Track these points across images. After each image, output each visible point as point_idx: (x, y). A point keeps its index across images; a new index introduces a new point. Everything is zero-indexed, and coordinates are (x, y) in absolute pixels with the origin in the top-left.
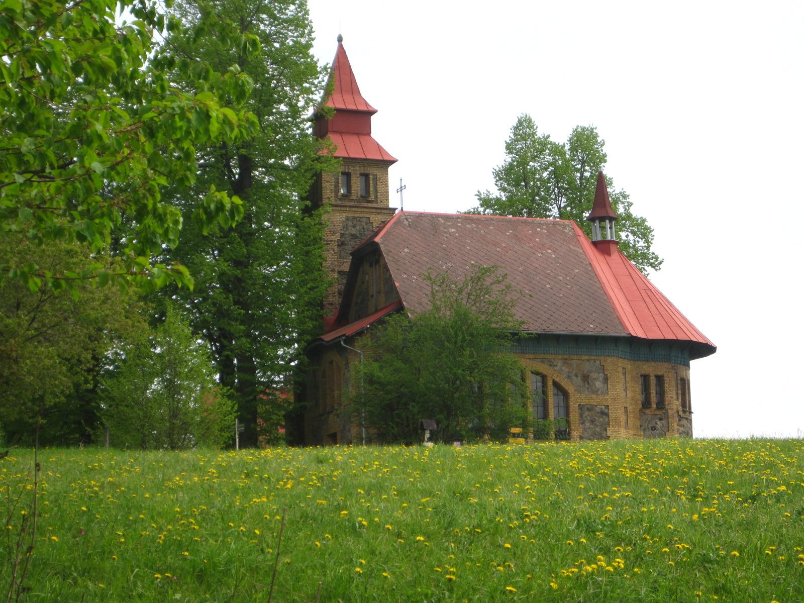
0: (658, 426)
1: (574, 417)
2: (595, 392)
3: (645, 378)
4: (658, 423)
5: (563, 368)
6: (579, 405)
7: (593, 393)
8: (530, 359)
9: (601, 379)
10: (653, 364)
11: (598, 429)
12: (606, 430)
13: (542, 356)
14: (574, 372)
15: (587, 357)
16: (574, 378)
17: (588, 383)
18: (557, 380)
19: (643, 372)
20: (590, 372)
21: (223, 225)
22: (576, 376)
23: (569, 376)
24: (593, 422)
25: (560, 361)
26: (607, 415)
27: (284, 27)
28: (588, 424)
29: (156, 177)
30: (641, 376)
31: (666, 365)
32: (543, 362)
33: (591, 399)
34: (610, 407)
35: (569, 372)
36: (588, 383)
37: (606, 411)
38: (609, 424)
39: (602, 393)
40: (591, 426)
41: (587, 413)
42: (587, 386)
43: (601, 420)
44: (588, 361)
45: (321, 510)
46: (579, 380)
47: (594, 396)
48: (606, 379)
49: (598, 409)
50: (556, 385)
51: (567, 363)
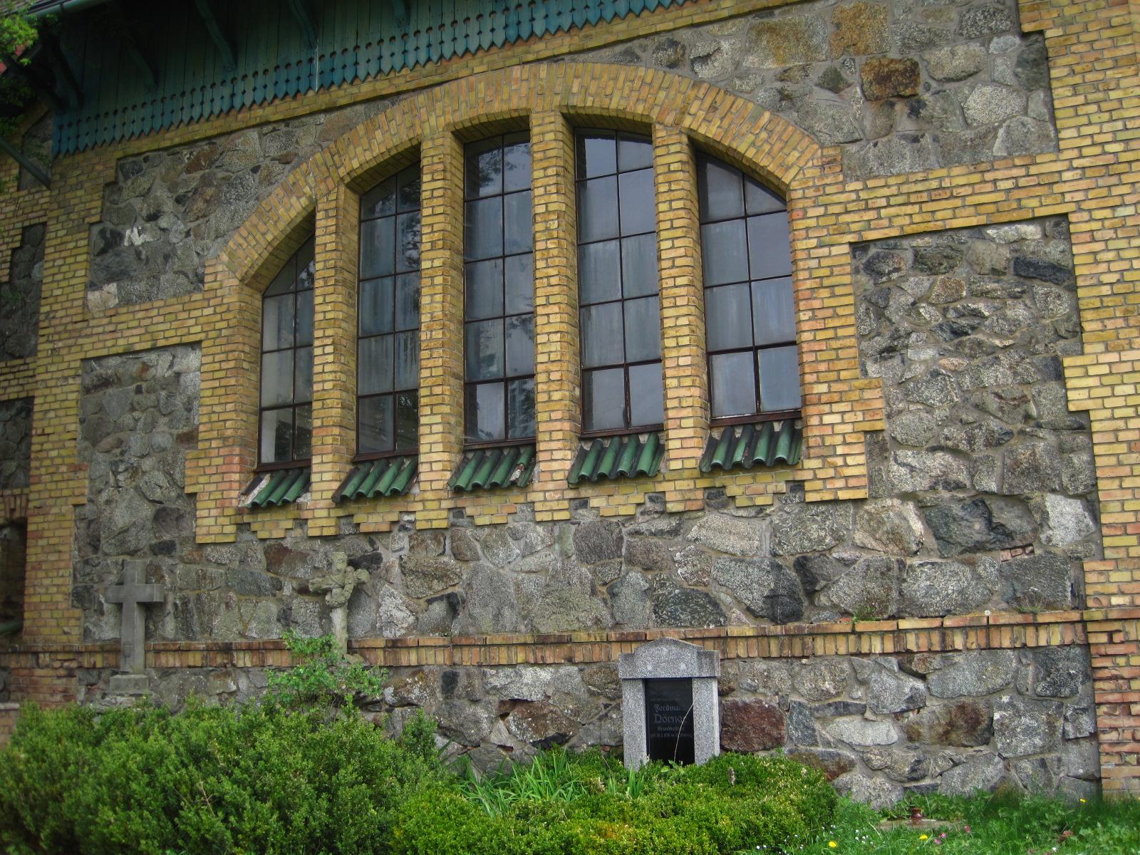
1: (825, 311)
2: (973, 149)
5: (751, 61)
6: (859, 247)
7: (948, 159)
8: (554, 59)
9: (1004, 68)
11: (997, 376)
12: (1058, 374)
13: (621, 29)
14: (819, 69)
16: (822, 97)
17: (916, 109)
18: (710, 131)
19: (535, 121)
20: (931, 44)
21: (473, 464)
22: (834, 83)
23: (784, 96)
24: (957, 333)
25: (730, 27)
26: (1062, 275)
27: (150, 680)
28: (922, 355)
32: (627, 51)
34: (1079, 224)
35: (784, 76)
36: (916, 109)
37: (1054, 251)
38: (1077, 331)
39: (1016, 147)
40: (950, 362)
41: (916, 284)
42: (907, 125)
43: (1019, 311)
47: (959, 176)
48: (1036, 65)
49: (993, 249)
51: (771, 30)
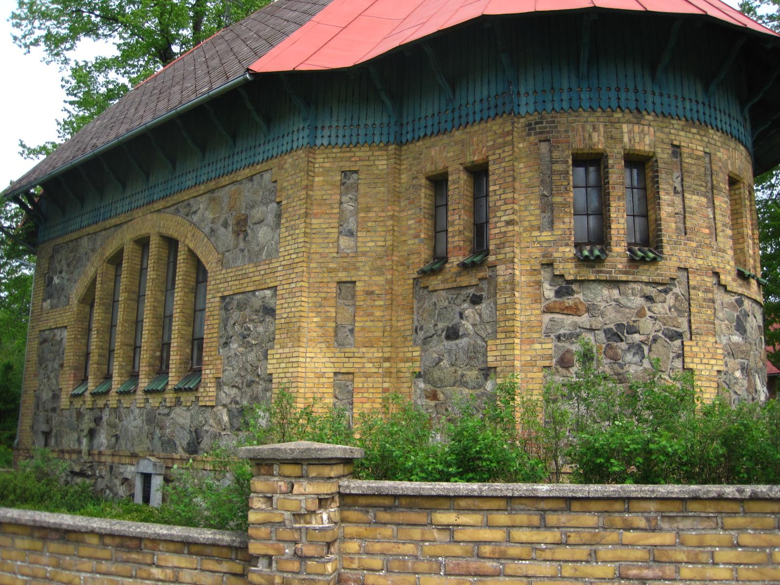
0: (467, 325)
3: (439, 182)
4: (469, 312)
8: (159, 211)
10: (458, 134)
15: (247, 172)
18: (191, 246)
19: (429, 168)
20: (252, 207)
22: (225, 225)
29: (716, 291)
30: (429, 178)
31: (496, 126)
33: (245, 276)
42: (242, 245)
43: (261, 329)
44: (251, 178)
45: (671, 416)
46: (226, 236)
49: (257, 303)
50: (192, 254)
